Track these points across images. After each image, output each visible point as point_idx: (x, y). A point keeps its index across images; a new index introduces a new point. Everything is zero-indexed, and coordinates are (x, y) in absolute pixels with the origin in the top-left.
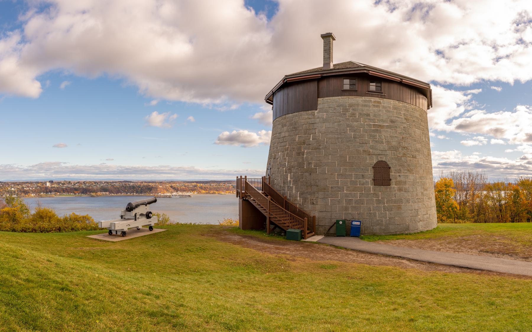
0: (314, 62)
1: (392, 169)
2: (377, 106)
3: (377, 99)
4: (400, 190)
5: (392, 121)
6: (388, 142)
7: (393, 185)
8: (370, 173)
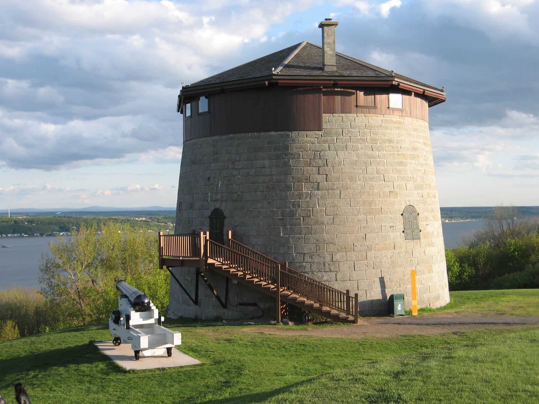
2: (399, 128)
5: (415, 149)
7: (422, 240)
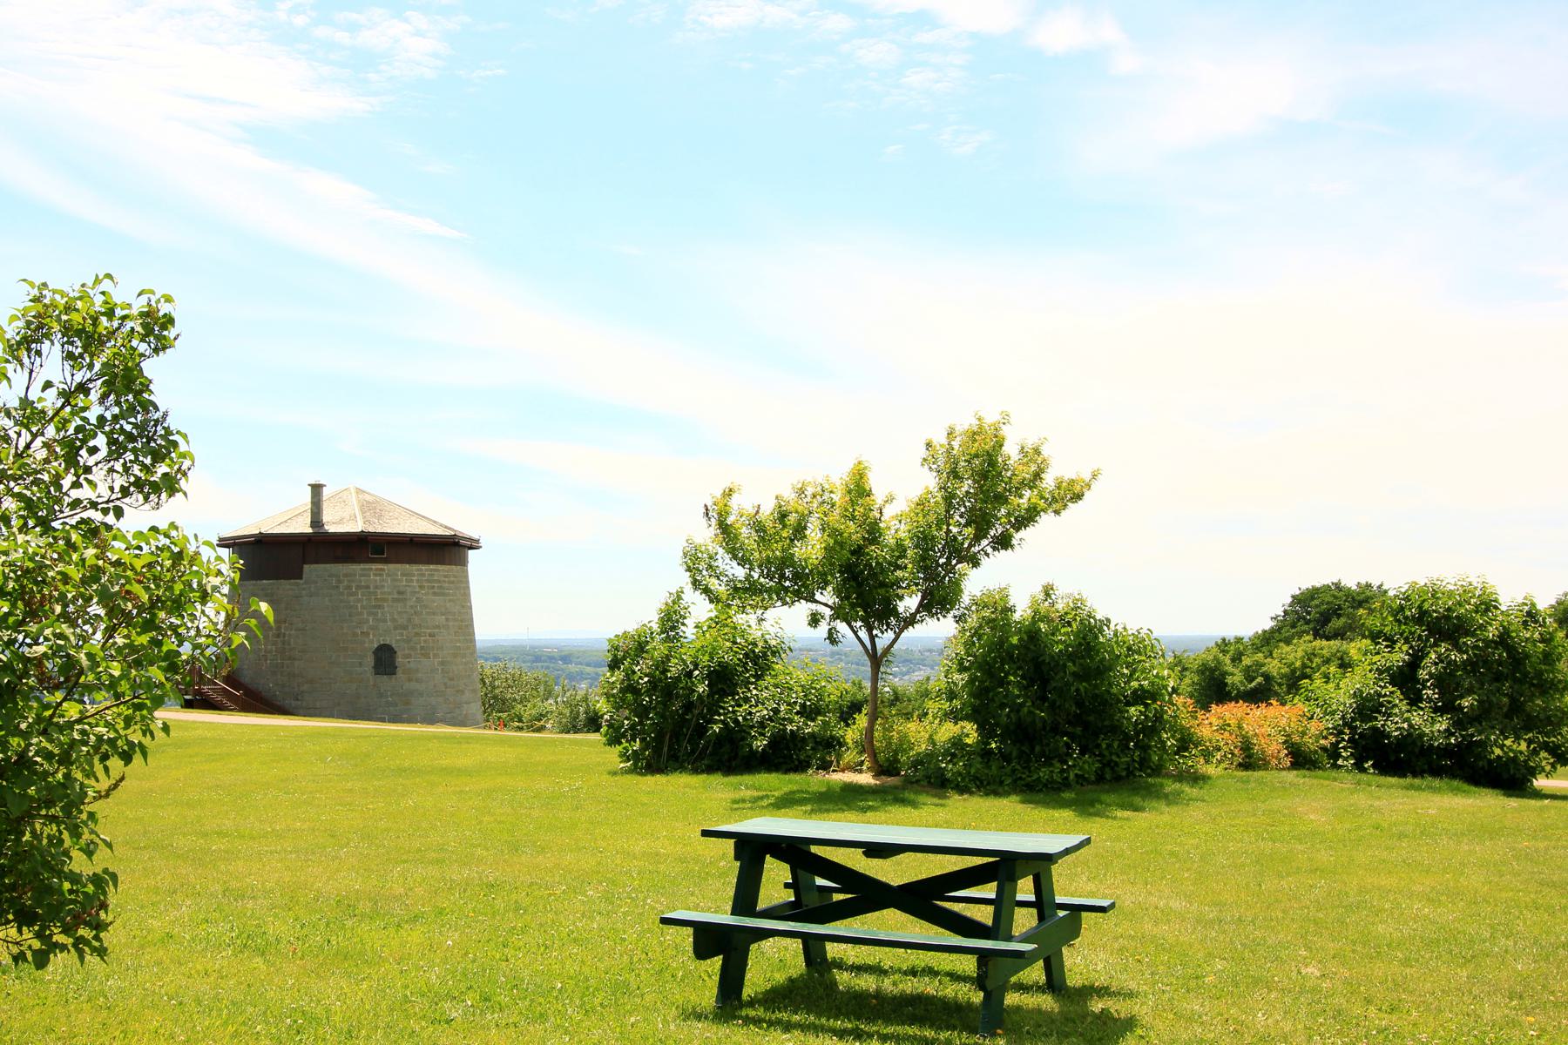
1: (399, 654)
4: (410, 680)
5: (399, 593)
6: (394, 620)
8: (370, 660)
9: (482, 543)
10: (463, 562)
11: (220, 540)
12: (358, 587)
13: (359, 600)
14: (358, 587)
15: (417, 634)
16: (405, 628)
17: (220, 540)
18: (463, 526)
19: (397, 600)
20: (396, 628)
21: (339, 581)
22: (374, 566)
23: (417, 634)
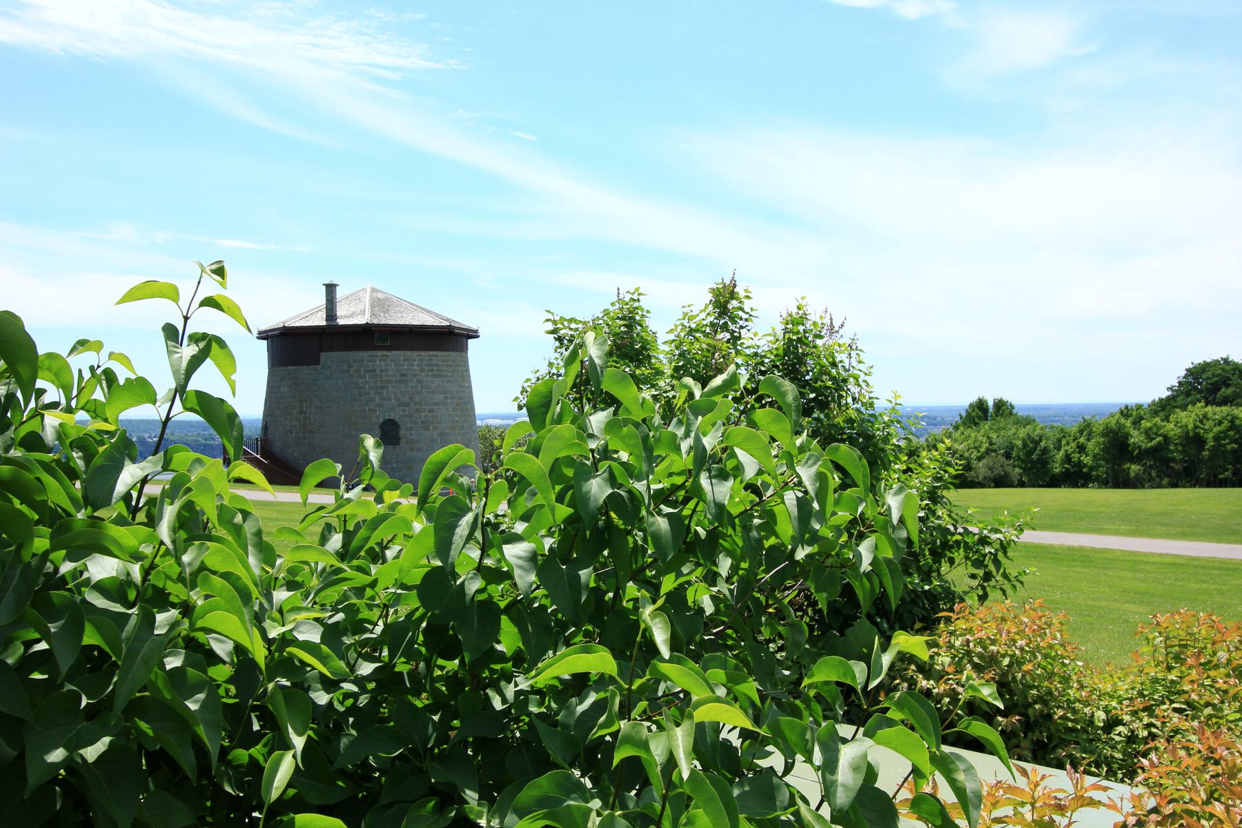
0: (304, 310)
1: (402, 427)
3: (385, 353)
5: (402, 375)
6: (397, 399)
9: (481, 333)
10: (464, 349)
11: (260, 333)
12: (366, 371)
13: (366, 383)
14: (366, 371)
15: (418, 411)
16: (407, 405)
17: (260, 333)
18: (464, 320)
19: (400, 381)
20: (399, 405)
21: (351, 366)
22: (380, 353)
23: (418, 411)
